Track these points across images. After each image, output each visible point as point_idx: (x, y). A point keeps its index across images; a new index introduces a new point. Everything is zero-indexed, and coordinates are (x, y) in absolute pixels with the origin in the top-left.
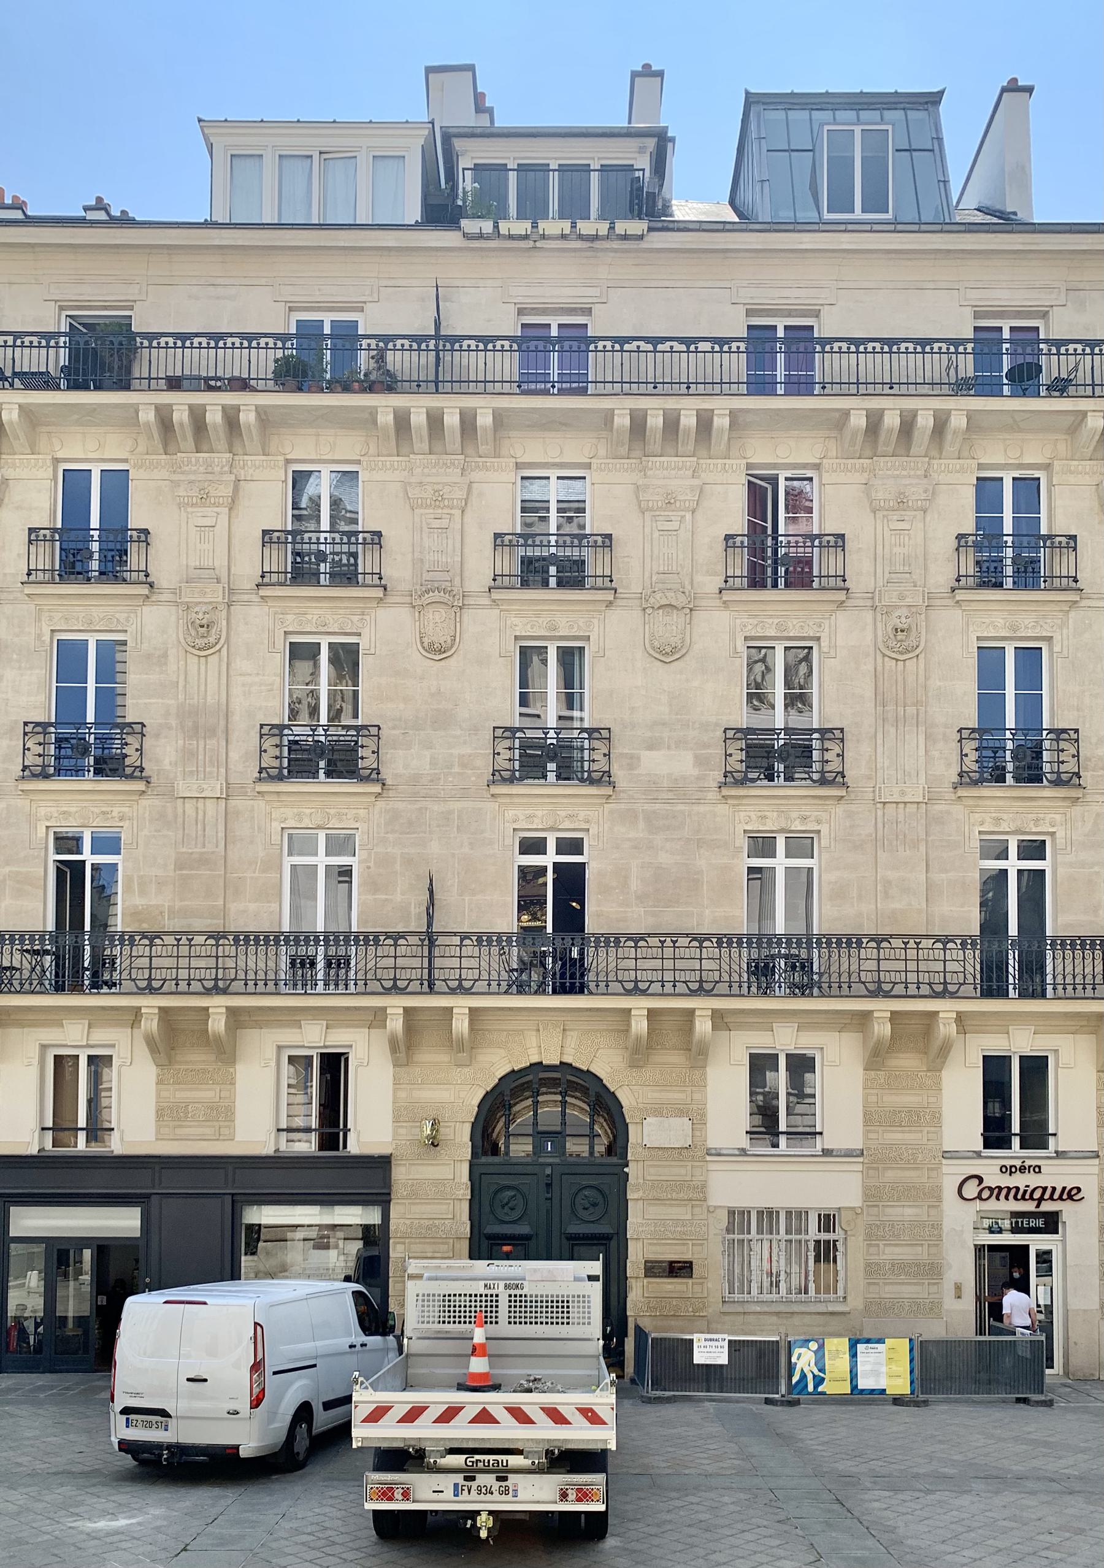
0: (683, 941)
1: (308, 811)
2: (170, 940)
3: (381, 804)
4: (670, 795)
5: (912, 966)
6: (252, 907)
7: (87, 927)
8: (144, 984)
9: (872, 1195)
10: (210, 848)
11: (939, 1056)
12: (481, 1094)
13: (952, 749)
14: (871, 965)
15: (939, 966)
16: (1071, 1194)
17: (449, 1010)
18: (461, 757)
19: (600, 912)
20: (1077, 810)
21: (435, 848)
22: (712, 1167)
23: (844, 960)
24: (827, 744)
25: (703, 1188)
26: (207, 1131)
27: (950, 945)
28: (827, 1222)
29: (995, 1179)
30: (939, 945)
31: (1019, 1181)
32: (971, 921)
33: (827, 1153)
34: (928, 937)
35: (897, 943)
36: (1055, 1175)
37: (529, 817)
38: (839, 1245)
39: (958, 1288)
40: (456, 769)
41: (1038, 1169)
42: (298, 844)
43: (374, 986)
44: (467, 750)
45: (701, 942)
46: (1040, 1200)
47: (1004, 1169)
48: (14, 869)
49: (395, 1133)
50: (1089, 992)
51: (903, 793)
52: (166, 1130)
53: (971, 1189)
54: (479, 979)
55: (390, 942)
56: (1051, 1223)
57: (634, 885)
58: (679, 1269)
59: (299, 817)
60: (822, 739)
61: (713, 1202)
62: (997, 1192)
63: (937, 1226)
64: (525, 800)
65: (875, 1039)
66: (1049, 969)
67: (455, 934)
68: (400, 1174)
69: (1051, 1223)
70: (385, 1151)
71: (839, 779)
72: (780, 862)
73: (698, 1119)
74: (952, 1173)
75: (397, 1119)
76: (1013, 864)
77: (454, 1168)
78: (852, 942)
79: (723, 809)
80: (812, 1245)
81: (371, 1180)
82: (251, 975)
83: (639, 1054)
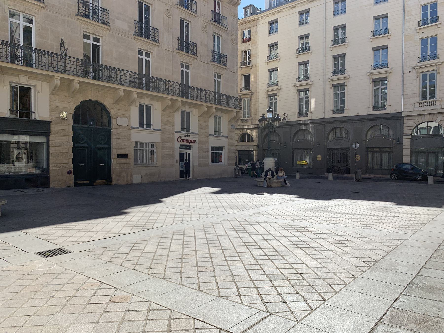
1: (18, 5)
3: (43, 10)
4: (122, 33)
8: (56, 69)
9: (163, 140)
11: (132, 103)
12: (75, 106)
13: (133, 25)
14: (167, 87)
16: (194, 142)
17: (72, 81)
19: (104, 60)
20: (195, 61)
22: (132, 131)
25: (130, 136)
28: (153, 146)
29: (183, 138)
31: (187, 138)
33: (154, 129)
36: (192, 138)
37: (87, 28)
38: (155, 151)
39: (177, 161)
40: (66, 7)
41: (189, 136)
42: (87, 37)
43: (51, 69)
46: (190, 143)
47: (185, 136)
49: (51, 115)
50: (47, 68)
51: (169, 48)
53: (179, 140)
54: (3, 57)
55: (119, 71)
56: (190, 147)
58: (124, 156)
61: (132, 140)
62: (183, 140)
64: (87, 23)
65: (55, 84)
66: (34, 58)
67: (75, 58)
68: (52, 127)
69: (190, 147)
70: (48, 120)
73: (129, 119)
74: (177, 136)
75: (51, 111)
76: (91, 42)
77: (68, 127)
78: (158, 79)
79: (134, 41)
80: (150, 151)
81: (43, 128)
83: (118, 101)
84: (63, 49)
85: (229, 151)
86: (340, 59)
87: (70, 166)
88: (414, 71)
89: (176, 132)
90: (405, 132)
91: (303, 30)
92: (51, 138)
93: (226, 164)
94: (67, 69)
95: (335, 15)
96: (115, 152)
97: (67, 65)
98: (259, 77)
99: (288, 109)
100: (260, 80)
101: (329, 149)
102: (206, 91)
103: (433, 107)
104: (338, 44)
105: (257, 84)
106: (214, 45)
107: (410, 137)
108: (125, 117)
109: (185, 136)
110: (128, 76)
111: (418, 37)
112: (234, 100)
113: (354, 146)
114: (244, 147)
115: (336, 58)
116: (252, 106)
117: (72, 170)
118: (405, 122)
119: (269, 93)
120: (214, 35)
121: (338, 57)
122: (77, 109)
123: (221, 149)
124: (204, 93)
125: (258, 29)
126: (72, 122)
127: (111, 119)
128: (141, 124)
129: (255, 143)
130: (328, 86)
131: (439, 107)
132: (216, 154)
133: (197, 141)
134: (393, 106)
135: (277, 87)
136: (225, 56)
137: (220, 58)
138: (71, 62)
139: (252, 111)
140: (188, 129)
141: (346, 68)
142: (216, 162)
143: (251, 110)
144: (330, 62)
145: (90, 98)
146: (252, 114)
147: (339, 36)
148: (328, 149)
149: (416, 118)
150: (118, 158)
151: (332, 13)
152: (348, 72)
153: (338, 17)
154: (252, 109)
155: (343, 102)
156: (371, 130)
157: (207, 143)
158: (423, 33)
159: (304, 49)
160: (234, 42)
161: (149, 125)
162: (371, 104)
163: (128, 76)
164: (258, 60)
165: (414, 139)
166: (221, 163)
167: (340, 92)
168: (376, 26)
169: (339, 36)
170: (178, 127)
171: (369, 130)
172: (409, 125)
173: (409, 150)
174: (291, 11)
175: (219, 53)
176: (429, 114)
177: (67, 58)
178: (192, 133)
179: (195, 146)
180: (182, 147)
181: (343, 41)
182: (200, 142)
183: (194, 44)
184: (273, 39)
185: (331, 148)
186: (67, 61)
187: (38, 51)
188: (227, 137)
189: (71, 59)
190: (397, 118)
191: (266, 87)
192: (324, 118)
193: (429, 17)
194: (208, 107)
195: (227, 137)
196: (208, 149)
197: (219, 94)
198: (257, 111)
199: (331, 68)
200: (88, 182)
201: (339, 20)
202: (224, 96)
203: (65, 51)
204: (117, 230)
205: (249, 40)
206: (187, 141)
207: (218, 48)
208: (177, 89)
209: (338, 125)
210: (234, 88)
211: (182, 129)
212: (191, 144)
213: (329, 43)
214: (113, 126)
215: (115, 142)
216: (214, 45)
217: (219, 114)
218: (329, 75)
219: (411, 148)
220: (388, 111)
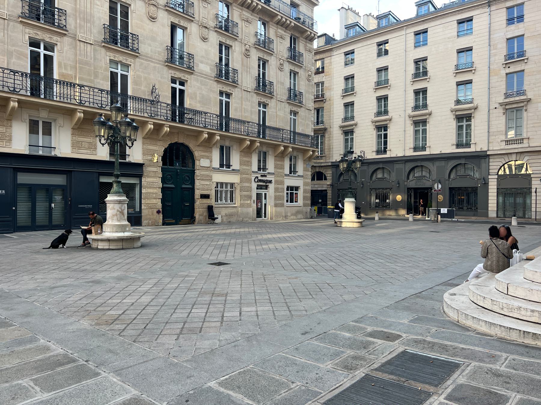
0: (214, 116)
2: (87, 88)
5: (91, 97)
6: (101, 82)
7: (178, 104)
8: (100, 105)
9: (241, 181)
10: (89, 59)
14: (203, 119)
15: (12, 81)
16: (270, 182)
18: (158, 51)
21: (152, 76)
23: (65, 90)
24: (60, 14)
26: (89, 151)
27: (103, 92)
29: (260, 178)
30: (100, 92)
32: (107, 86)
33: (233, 170)
34: (8, 69)
35: (251, 124)
36: (269, 178)
41: (266, 176)
44: (160, 50)
45: (15, 73)
48: (17, 49)
52: (74, 150)
53: (256, 180)
57: (198, 98)
59: (115, 57)
60: (58, 12)
61: (213, 181)
63: (251, 188)
69: (266, 187)
70: (141, 162)
71: (65, 28)
72: (42, 51)
81: (136, 170)
82: (69, 96)
84: (154, 95)
85: (305, 191)
87: (159, 205)
88: (500, 107)
89: (253, 172)
90: (490, 171)
91: (382, 62)
92: (143, 180)
93: (301, 204)
94: (159, 113)
96: (197, 193)
97: (159, 110)
98: (333, 111)
99: (365, 145)
101: (409, 189)
102: (283, 130)
103: (520, 146)
104: (419, 77)
105: (331, 118)
106: (291, 82)
107: (496, 177)
108: (208, 158)
109: (262, 176)
110: (212, 118)
111: (504, 72)
112: (310, 139)
114: (316, 186)
116: (326, 142)
117: (161, 210)
118: (491, 160)
120: (291, 72)
121: (419, 92)
122: (165, 151)
123: (297, 188)
124: (281, 132)
125: (332, 60)
126: (161, 164)
127: (194, 161)
128: (222, 165)
129: (329, 182)
130: (409, 123)
131: (527, 145)
133: (273, 181)
134: (479, 143)
136: (301, 93)
137: (296, 96)
138: (162, 108)
139: (326, 147)
140: (265, 169)
143: (325, 146)
144: (411, 96)
145: (176, 141)
146: (326, 150)
147: (420, 69)
148: (408, 188)
149: (503, 156)
151: (413, 45)
153: (418, 49)
154: (326, 145)
157: (282, 183)
158: (509, 67)
159: (382, 83)
160: (310, 79)
161: (229, 166)
163: (212, 118)
164: (332, 93)
165: (501, 178)
166: (296, 203)
169: (420, 69)
170: (255, 168)
172: (494, 164)
173: (496, 190)
174: (369, 42)
175: (295, 90)
176: (517, 153)
177: (159, 104)
178: (269, 173)
179: (271, 187)
180: (259, 187)
184: (349, 71)
185: (412, 188)
186: (159, 107)
187: (134, 98)
188: (302, 176)
189: (162, 104)
190: (482, 157)
191: (341, 122)
192: (404, 156)
193: (516, 51)
194: (285, 147)
195: (302, 176)
196: (284, 189)
197: (295, 133)
198: (331, 147)
199: (411, 103)
200: (174, 221)
201: (420, 53)
202: (300, 134)
203: (157, 96)
204: (126, 292)
205: (323, 72)
207: (295, 85)
208: (255, 130)
211: (259, 169)
212: (267, 184)
213: (410, 77)
214: (197, 167)
216: (291, 82)
217: (295, 154)
218: (410, 112)
219: (497, 189)
220: (472, 149)
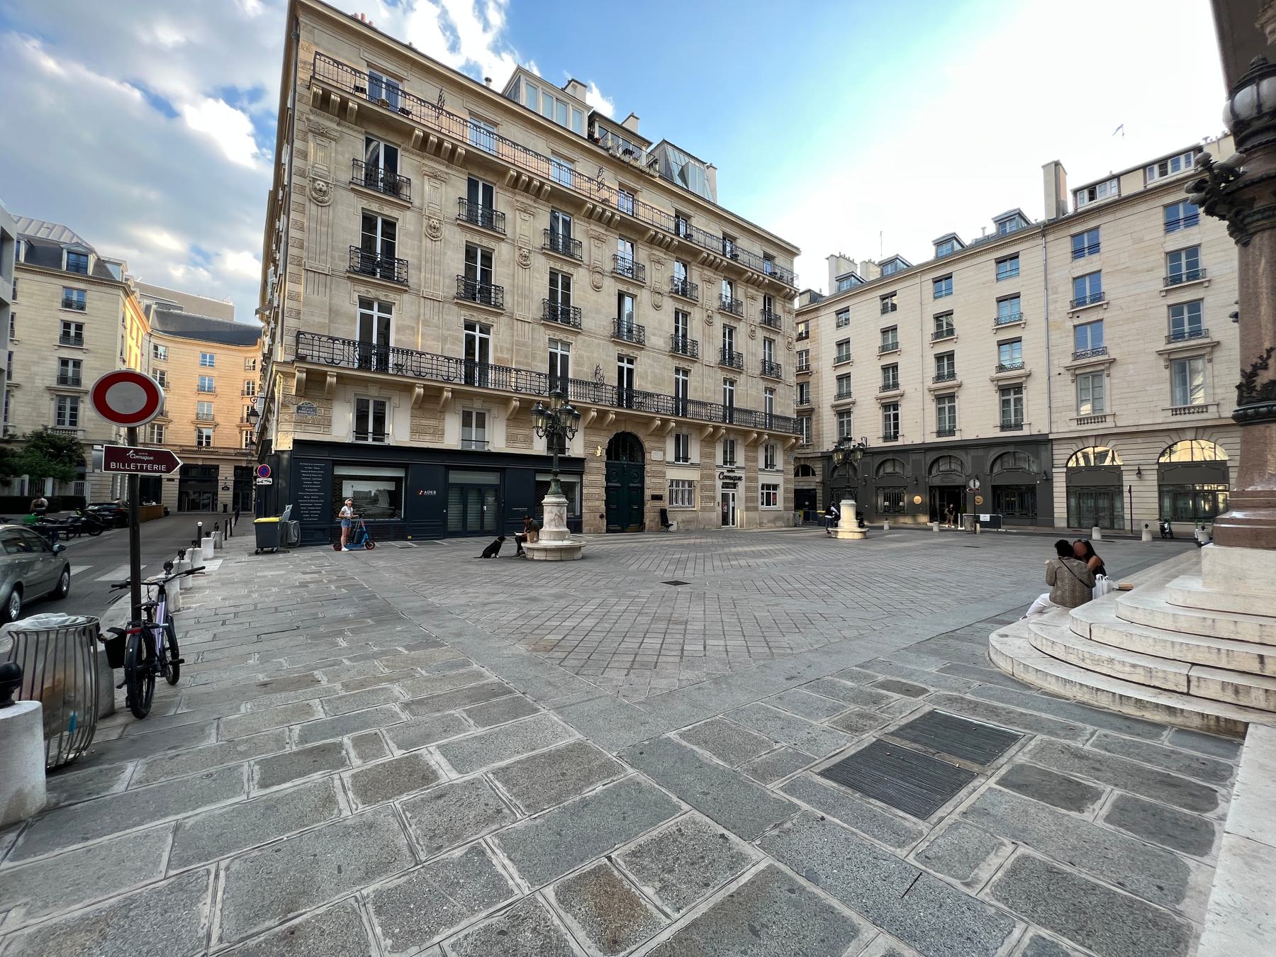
16: (740, 479)
31: (731, 474)
62: (726, 477)
69: (735, 486)
85: (786, 490)
86: (946, 359)
95: (935, 298)
96: (648, 493)
99: (868, 429)
100: (825, 392)
103: (1101, 425)
113: (978, 484)
115: (939, 358)
119: (1001, 383)
123: (775, 487)
128: (677, 459)
130: (929, 398)
132: (768, 494)
134: (1035, 422)
135: (1022, 371)
140: (732, 462)
141: (900, 380)
142: (768, 504)
150: (993, 487)
152: (959, 379)
155: (896, 426)
156: (999, 462)
157: (756, 480)
161: (686, 459)
162: (998, 422)
167: (892, 412)
168: (839, 352)
170: (719, 461)
171: (995, 461)
173: (1156, 488)
180: (725, 486)
181: (951, 332)
182: (747, 478)
183: (740, 355)
190: (1041, 443)
197: (771, 415)
206: (730, 478)
209: (1011, 449)
210: (786, 405)
211: (725, 463)
215: (648, 481)
217: (772, 442)
218: (930, 383)
219: (1159, 486)
220: (1025, 431)
